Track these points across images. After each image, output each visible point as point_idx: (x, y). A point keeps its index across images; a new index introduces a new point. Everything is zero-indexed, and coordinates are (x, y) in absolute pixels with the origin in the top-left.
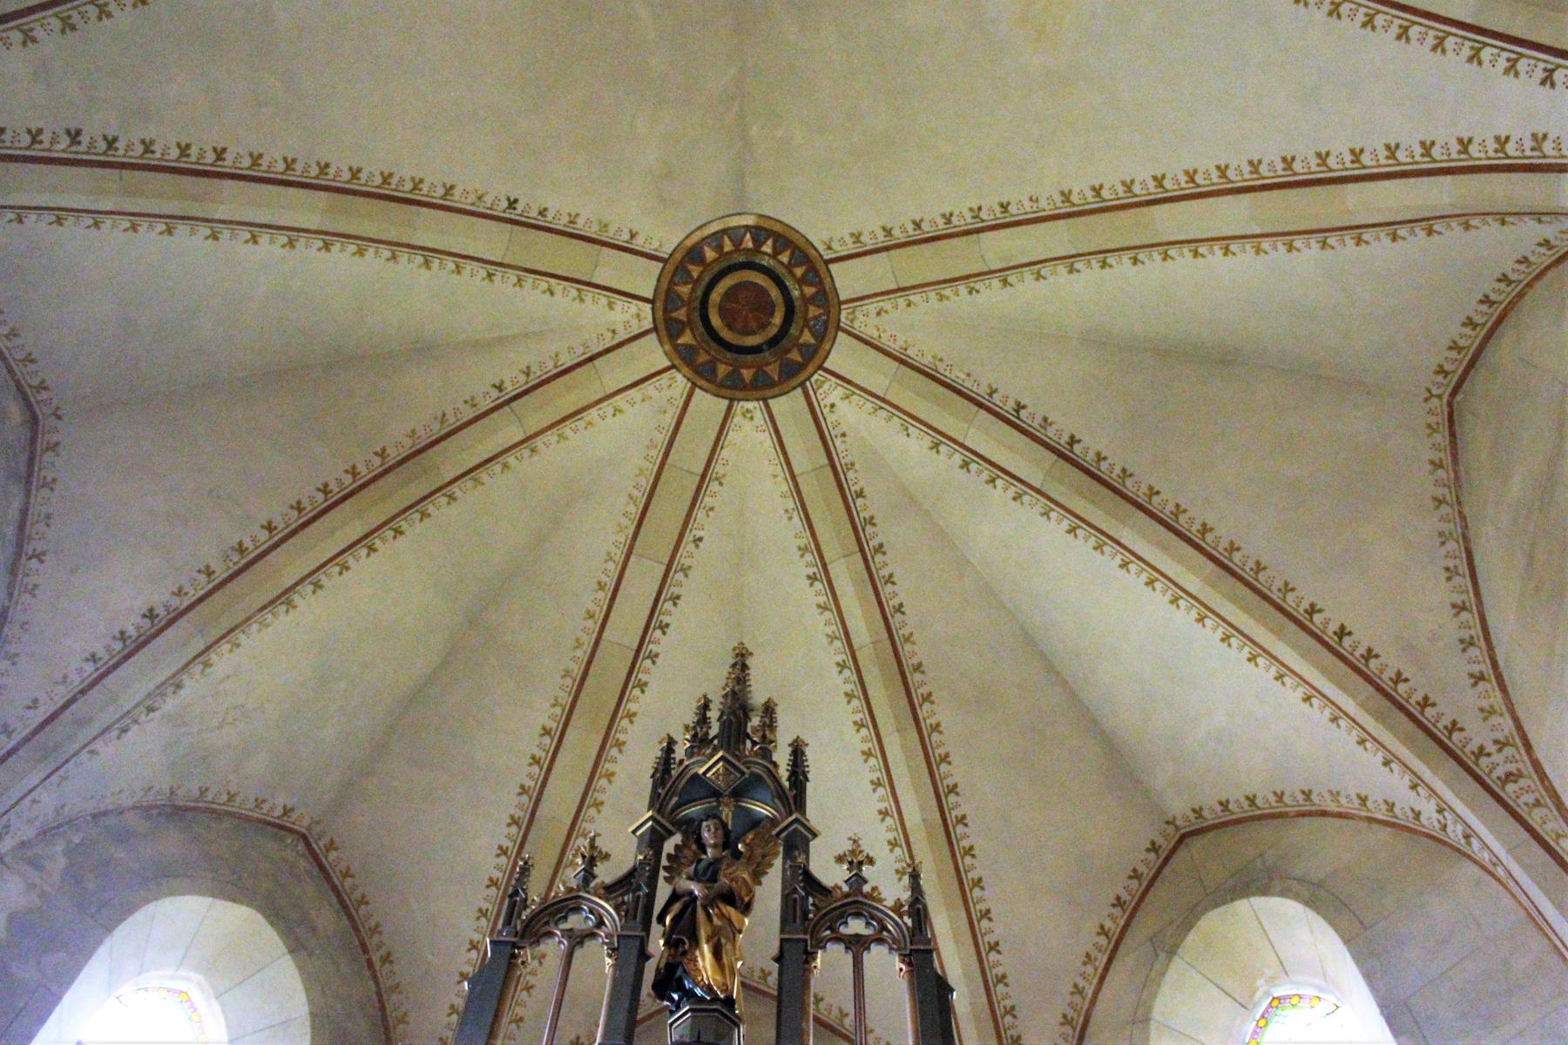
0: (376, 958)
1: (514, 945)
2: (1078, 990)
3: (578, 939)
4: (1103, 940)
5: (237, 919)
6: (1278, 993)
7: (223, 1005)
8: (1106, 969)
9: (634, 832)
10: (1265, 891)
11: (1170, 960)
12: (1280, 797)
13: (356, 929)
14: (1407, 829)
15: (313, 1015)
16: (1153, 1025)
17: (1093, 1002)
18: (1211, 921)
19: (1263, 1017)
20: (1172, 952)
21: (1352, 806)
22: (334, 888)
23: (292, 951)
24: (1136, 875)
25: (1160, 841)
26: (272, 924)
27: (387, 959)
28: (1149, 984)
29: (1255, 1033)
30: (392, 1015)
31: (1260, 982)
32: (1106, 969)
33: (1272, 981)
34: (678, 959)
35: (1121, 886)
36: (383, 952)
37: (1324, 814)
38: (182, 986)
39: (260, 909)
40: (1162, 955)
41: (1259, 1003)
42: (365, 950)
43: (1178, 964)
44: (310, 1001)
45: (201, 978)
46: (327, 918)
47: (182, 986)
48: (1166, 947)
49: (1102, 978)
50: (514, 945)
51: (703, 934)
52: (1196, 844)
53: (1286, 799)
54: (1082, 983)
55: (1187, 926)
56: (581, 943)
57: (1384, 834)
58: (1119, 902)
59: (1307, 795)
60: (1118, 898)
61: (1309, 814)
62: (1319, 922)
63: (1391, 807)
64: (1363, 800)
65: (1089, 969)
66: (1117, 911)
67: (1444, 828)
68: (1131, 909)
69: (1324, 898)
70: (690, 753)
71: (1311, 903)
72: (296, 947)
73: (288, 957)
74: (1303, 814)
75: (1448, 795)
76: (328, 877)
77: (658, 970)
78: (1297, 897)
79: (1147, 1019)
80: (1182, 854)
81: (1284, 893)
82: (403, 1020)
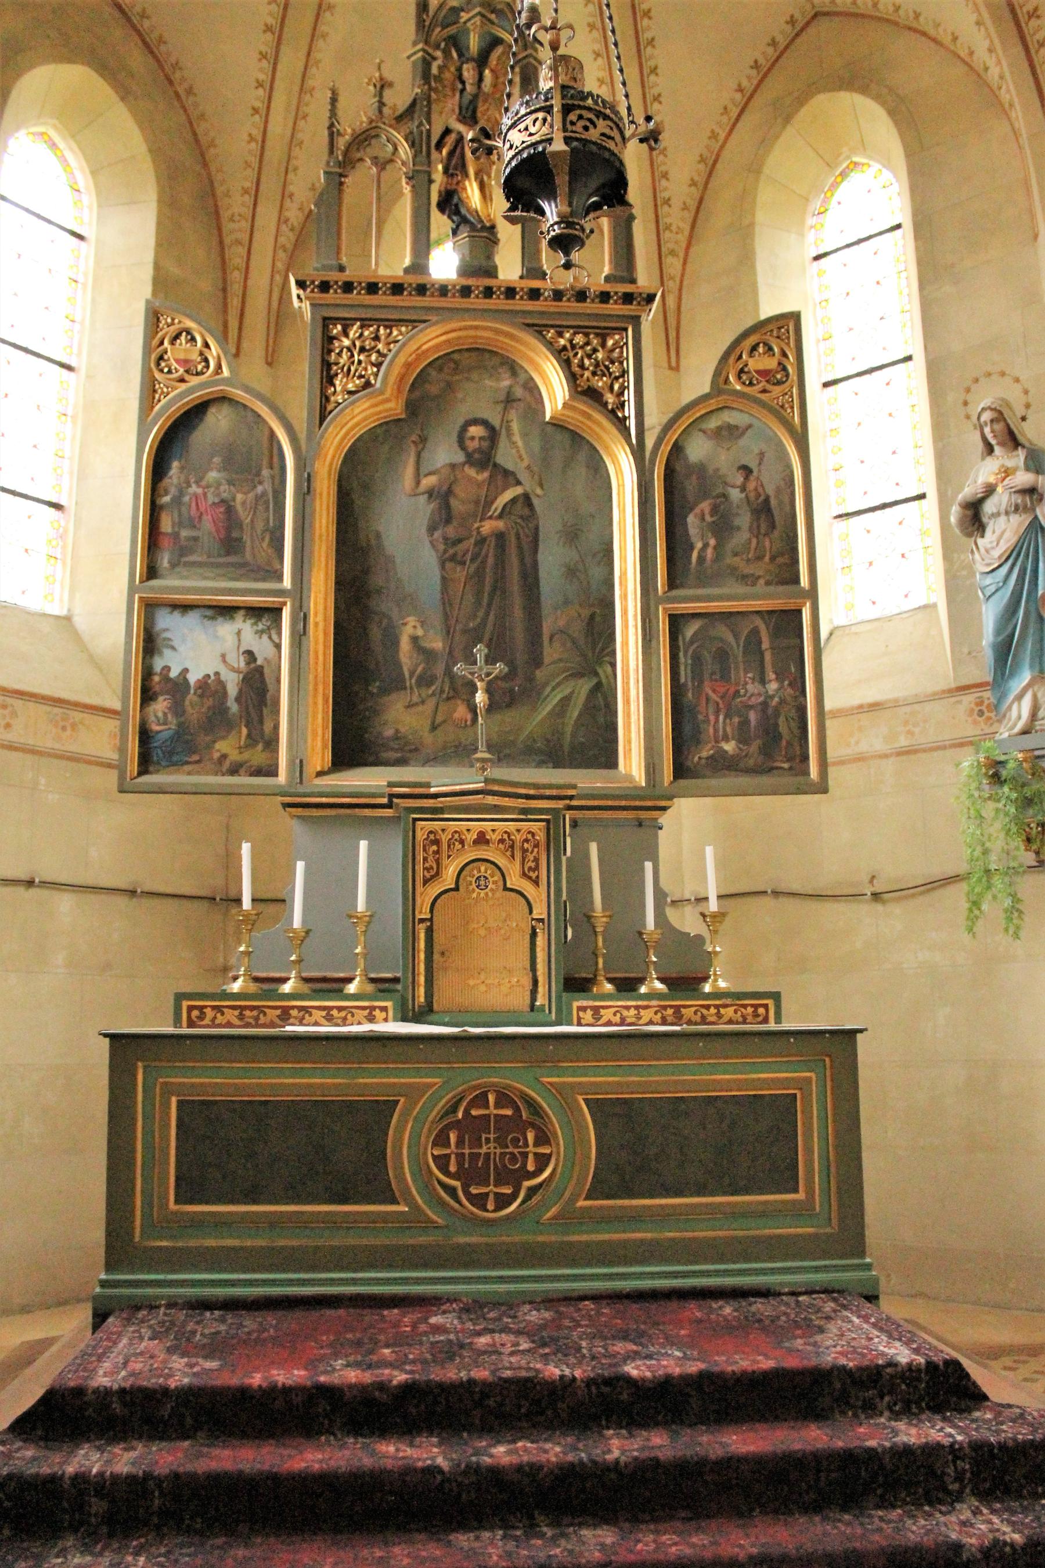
0: (181, 91)
1: (341, 175)
2: (714, 136)
3: (382, 164)
4: (738, 96)
5: (75, 75)
6: (855, 159)
7: (76, 142)
8: (737, 120)
9: (409, 57)
10: (864, 90)
11: (784, 127)
12: (897, 9)
13: (161, 67)
14: (977, 74)
15: (150, 151)
16: (763, 177)
17: (722, 147)
18: (821, 101)
19: (841, 174)
20: (788, 120)
21: (947, 40)
22: (134, 27)
23: (122, 99)
24: (773, 43)
25: (798, 15)
26: (102, 75)
27: (190, 91)
28: (766, 142)
29: (832, 185)
30: (204, 141)
31: (845, 149)
32: (737, 120)
33: (854, 151)
34: (454, 187)
35: (762, 52)
36: (186, 85)
37: (924, 34)
38: (42, 129)
39: (89, 64)
40: (779, 120)
41: (841, 164)
42: (171, 82)
43: (790, 131)
44: (146, 140)
45: (56, 121)
46: (137, 59)
47: (42, 129)
48: (785, 113)
49: (734, 125)
50: (341, 175)
51: (471, 172)
52: (824, 23)
53: (901, 12)
54: (717, 130)
55: (802, 100)
56: (383, 168)
57: (962, 69)
58: (756, 65)
59: (917, 16)
60: (756, 62)
61: (915, 31)
62: (894, 131)
63: (971, 53)
64: (955, 39)
65: (725, 119)
66: (754, 72)
67: (1000, 88)
68: (764, 72)
69: (904, 114)
70: (519, 483)
71: (892, 113)
72: (125, 94)
73: (121, 104)
74: (910, 28)
75: (1007, 75)
76: (129, 20)
77: (440, 192)
78: (883, 104)
79: (758, 172)
80: (811, 30)
81: (878, 98)
82: (212, 144)
